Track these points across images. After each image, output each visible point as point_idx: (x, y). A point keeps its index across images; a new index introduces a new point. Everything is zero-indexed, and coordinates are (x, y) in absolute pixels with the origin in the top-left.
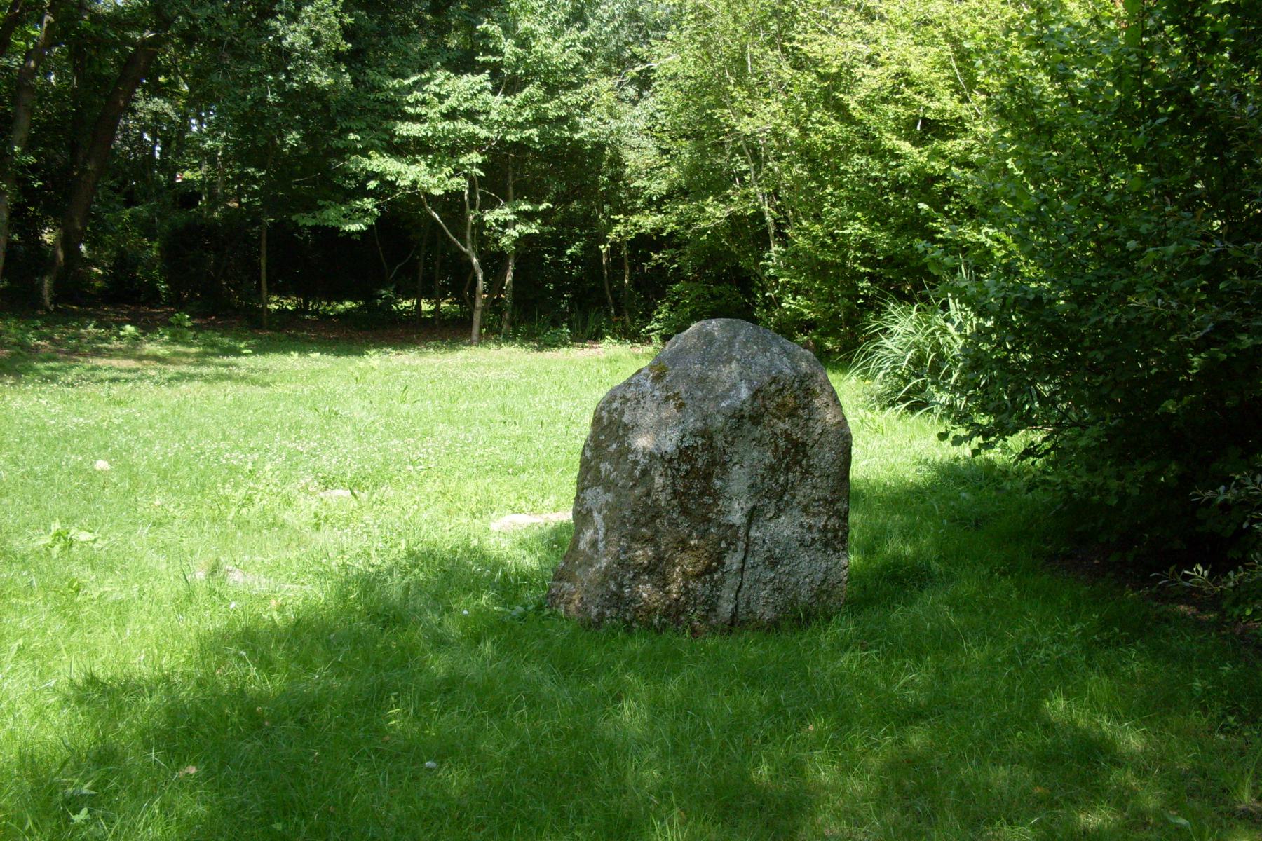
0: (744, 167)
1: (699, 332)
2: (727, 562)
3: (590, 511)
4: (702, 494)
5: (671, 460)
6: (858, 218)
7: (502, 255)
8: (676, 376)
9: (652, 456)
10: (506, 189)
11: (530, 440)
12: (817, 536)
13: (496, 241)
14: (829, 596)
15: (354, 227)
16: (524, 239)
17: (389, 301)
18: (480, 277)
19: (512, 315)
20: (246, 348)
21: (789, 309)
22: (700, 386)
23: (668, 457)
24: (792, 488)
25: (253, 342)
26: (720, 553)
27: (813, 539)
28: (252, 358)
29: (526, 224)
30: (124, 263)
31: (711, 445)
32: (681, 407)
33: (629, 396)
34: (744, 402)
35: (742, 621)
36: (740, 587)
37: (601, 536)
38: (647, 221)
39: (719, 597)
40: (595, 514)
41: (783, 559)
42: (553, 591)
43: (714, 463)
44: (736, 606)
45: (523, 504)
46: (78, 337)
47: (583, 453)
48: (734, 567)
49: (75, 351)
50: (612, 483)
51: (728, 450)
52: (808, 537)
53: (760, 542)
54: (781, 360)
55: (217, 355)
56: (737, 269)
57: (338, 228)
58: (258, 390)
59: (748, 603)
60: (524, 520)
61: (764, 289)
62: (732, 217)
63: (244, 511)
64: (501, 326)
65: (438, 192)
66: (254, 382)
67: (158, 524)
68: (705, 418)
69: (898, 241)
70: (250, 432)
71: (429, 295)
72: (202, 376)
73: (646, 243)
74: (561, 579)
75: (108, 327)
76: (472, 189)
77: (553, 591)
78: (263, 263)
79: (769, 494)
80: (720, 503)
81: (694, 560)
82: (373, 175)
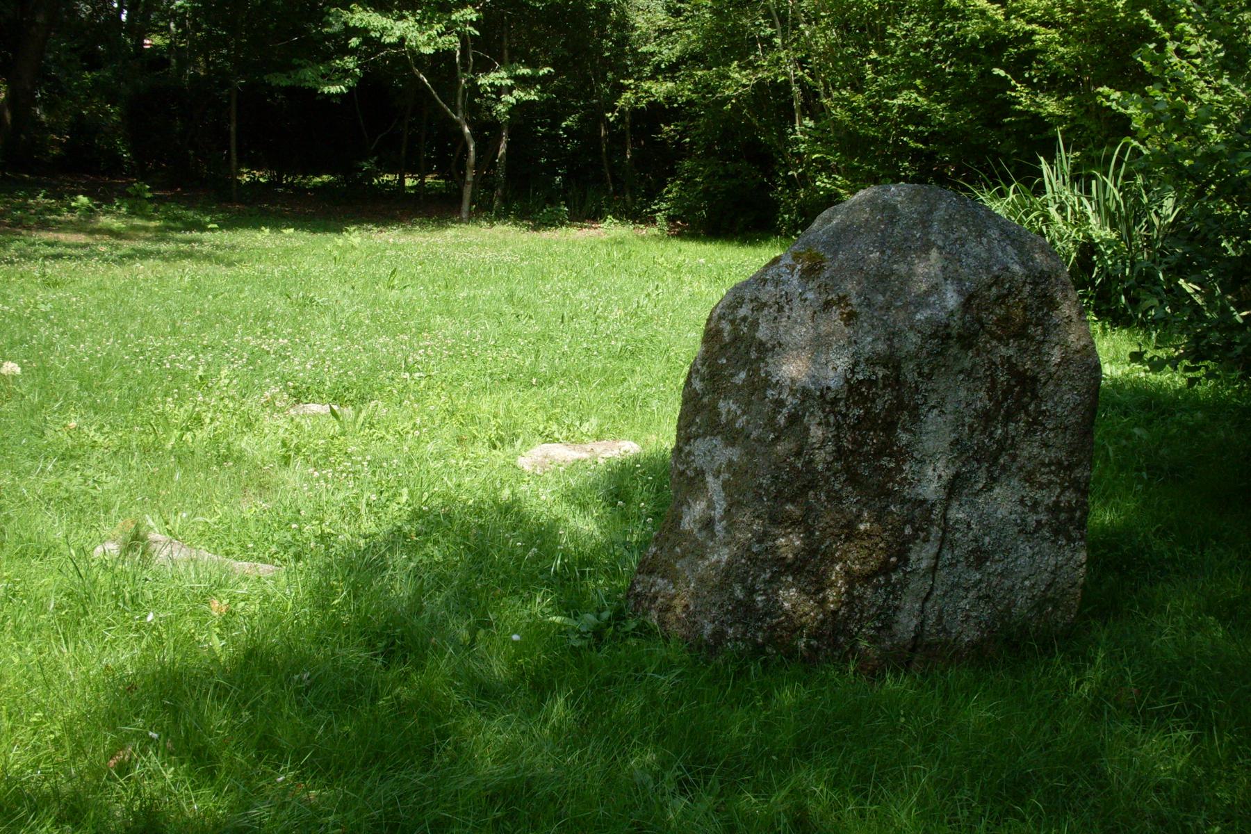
0: (769, 31)
1: (871, 201)
2: (913, 557)
3: (701, 473)
4: (879, 454)
5: (835, 401)
6: (916, 87)
7: (495, 126)
8: (840, 269)
9: (806, 393)
10: (501, 54)
11: (551, 339)
12: (1044, 518)
13: (489, 109)
14: (1056, 608)
15: (334, 89)
16: (521, 105)
17: (370, 175)
18: (472, 147)
19: (504, 191)
20: (211, 222)
21: (824, 189)
22: (880, 287)
23: (831, 395)
24: (1013, 446)
25: (220, 216)
26: (903, 544)
27: (1039, 522)
28: (218, 233)
29: (524, 90)
30: (81, 128)
31: (897, 380)
32: (850, 318)
33: (764, 298)
34: (952, 314)
35: (929, 645)
36: (929, 594)
37: (718, 512)
38: (660, 89)
39: (897, 608)
40: (710, 479)
41: (994, 552)
42: (639, 589)
43: (900, 406)
44: (922, 623)
45: (555, 427)
46: (25, 208)
47: (688, 382)
48: (924, 565)
49: (18, 223)
50: (739, 432)
51: (922, 387)
52: (1032, 519)
53: (962, 527)
54: (1004, 250)
55: (178, 230)
56: (755, 144)
57: (316, 90)
58: (223, 270)
59: (940, 618)
60: (563, 453)
61: (787, 167)
62: (760, 84)
63: (188, 436)
64: (492, 202)
65: (428, 50)
66: (219, 261)
67: (67, 457)
68: (891, 336)
69: (958, 114)
70: (206, 323)
71: (413, 170)
72: (159, 252)
73: (657, 112)
74: (651, 573)
75: (60, 197)
76: (464, 51)
77: (639, 589)
78: (232, 129)
79: (980, 455)
80: (906, 467)
81: (864, 553)
82: (355, 31)
